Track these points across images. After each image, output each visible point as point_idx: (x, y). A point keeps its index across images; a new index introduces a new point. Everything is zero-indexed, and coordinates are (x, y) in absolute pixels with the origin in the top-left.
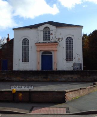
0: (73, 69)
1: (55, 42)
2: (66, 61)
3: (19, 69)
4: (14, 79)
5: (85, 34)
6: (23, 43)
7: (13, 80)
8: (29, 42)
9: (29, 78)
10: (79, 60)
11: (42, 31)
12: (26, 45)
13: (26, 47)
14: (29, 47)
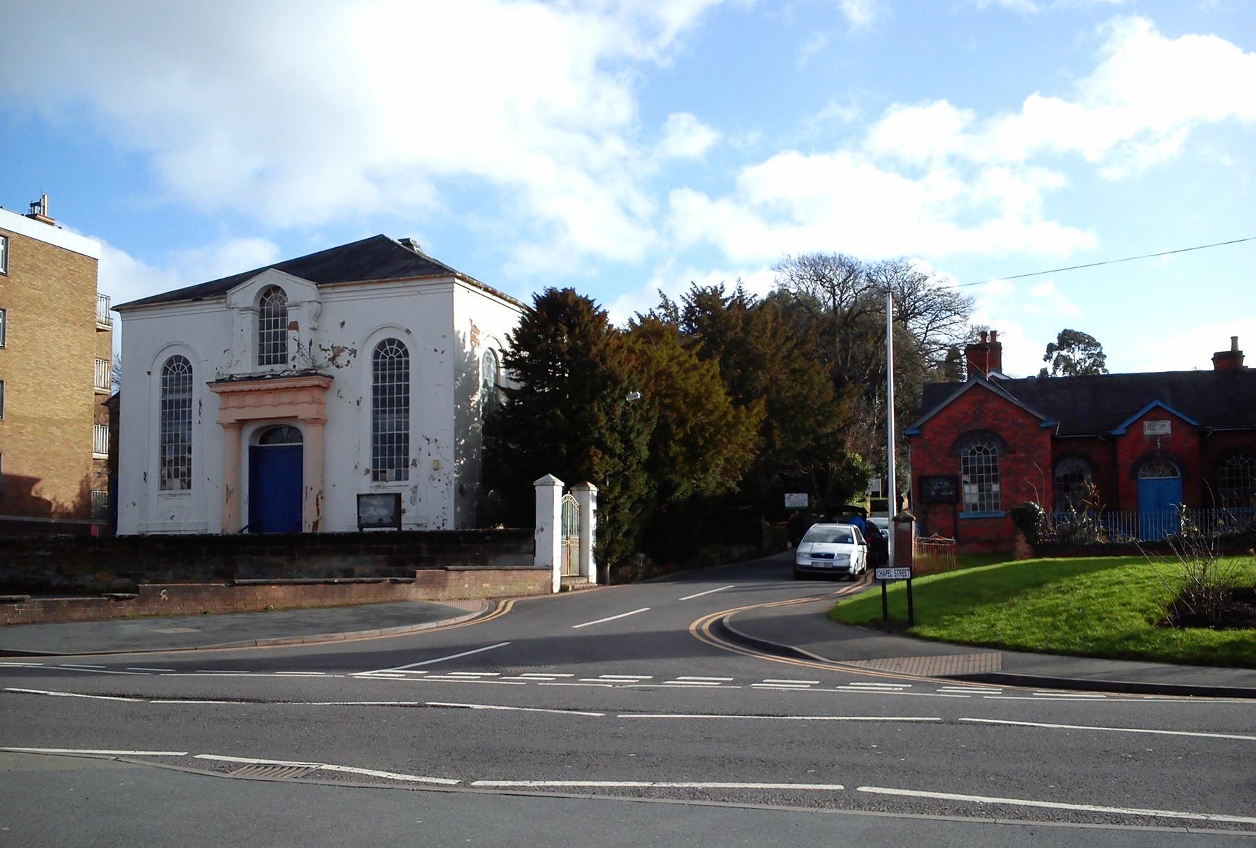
0: (361, 526)
1: (306, 374)
2: (375, 478)
4: (87, 580)
5: (590, 298)
10: (436, 474)
11: (246, 309)
12: (178, 391)
14: (190, 400)
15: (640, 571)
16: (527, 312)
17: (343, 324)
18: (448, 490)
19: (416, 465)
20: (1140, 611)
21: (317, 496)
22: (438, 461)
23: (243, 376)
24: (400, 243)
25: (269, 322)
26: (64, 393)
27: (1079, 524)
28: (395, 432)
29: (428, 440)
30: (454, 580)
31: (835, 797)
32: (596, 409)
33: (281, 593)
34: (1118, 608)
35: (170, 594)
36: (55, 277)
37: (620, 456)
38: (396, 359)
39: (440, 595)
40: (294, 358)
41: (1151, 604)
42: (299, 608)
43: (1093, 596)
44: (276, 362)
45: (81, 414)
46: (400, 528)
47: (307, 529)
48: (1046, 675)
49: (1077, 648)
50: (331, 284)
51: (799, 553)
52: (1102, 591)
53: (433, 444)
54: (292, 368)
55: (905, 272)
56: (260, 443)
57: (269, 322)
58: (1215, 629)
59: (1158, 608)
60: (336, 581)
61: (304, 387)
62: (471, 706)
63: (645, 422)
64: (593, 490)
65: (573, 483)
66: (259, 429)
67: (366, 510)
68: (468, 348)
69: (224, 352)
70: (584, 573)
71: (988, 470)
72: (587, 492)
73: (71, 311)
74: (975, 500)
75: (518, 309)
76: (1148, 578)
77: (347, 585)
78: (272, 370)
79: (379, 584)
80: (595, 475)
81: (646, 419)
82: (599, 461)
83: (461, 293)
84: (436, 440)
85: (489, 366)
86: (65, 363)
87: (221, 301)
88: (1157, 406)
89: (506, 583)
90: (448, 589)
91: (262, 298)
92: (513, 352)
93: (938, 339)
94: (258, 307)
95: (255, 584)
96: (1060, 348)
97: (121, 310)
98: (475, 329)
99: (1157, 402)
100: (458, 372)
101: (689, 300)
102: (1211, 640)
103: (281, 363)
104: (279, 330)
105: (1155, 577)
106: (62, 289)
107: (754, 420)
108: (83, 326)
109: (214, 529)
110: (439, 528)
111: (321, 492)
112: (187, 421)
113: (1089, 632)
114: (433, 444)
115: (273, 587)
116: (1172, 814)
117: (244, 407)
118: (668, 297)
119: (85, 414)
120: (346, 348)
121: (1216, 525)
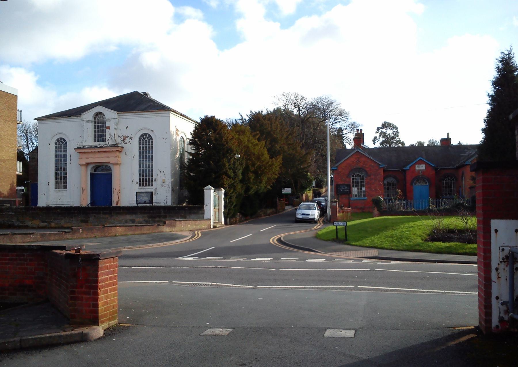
1: (113, 146)
2: (140, 185)
3: (48, 204)
4: (29, 223)
6: (56, 147)
7: (27, 226)
8: (154, 141)
9: (56, 221)
11: (89, 121)
12: (61, 151)
13: (61, 157)
14: (66, 155)
15: (238, 220)
16: (197, 124)
17: (127, 127)
18: (168, 190)
19: (156, 181)
20: (419, 236)
21: (118, 192)
22: (164, 179)
23: (88, 146)
24: (143, 94)
25: (98, 126)
26: (5, 149)
27: (395, 204)
28: (147, 168)
29: (161, 171)
30: (178, 224)
31: (353, 289)
32: (225, 161)
33: (120, 230)
34: (412, 235)
35: (83, 231)
36: (2, 103)
37: (232, 178)
38: (147, 141)
39: (174, 229)
40: (108, 140)
41: (422, 234)
42: (126, 235)
43: (404, 231)
44: (101, 141)
45: (12, 157)
46: (152, 204)
47: (114, 204)
48: (459, 260)
49: (400, 248)
50: (123, 112)
51: (297, 214)
52: (407, 230)
53: (162, 173)
54: (107, 144)
55: (324, 101)
56: (94, 171)
57: (98, 126)
58: (442, 242)
59: (425, 235)
60: (139, 225)
61: (113, 151)
62: (233, 267)
63: (241, 165)
64: (223, 191)
65: (217, 187)
66: (93, 167)
67: (139, 198)
68: (174, 137)
69: (80, 137)
70: (220, 221)
71: (361, 182)
72: (221, 191)
73: (8, 116)
74: (356, 193)
75: (194, 123)
76: (421, 225)
77: (143, 227)
78: (99, 144)
79: (153, 226)
80: (224, 185)
81: (241, 164)
82: (227, 181)
83: (173, 118)
84: (164, 172)
85: (181, 143)
86: (6, 137)
87: (79, 117)
88: (421, 159)
89: (195, 225)
90: (176, 227)
91: (95, 117)
92: (193, 139)
93: (337, 127)
94: (93, 120)
95: (112, 226)
96: (381, 128)
97: (38, 120)
98: (177, 130)
99: (420, 158)
100: (171, 146)
101: (250, 116)
102: (441, 246)
103: (103, 142)
104: (102, 129)
105: (423, 225)
106: (4, 108)
107: (278, 163)
108: (12, 122)
109: (77, 204)
110: (165, 204)
111: (119, 190)
112: (65, 163)
113: (404, 243)
114: (162, 173)
115: (118, 227)
116: (436, 291)
117: (89, 158)
118: (243, 116)
119: (14, 157)
120: (128, 136)
121: (441, 205)
